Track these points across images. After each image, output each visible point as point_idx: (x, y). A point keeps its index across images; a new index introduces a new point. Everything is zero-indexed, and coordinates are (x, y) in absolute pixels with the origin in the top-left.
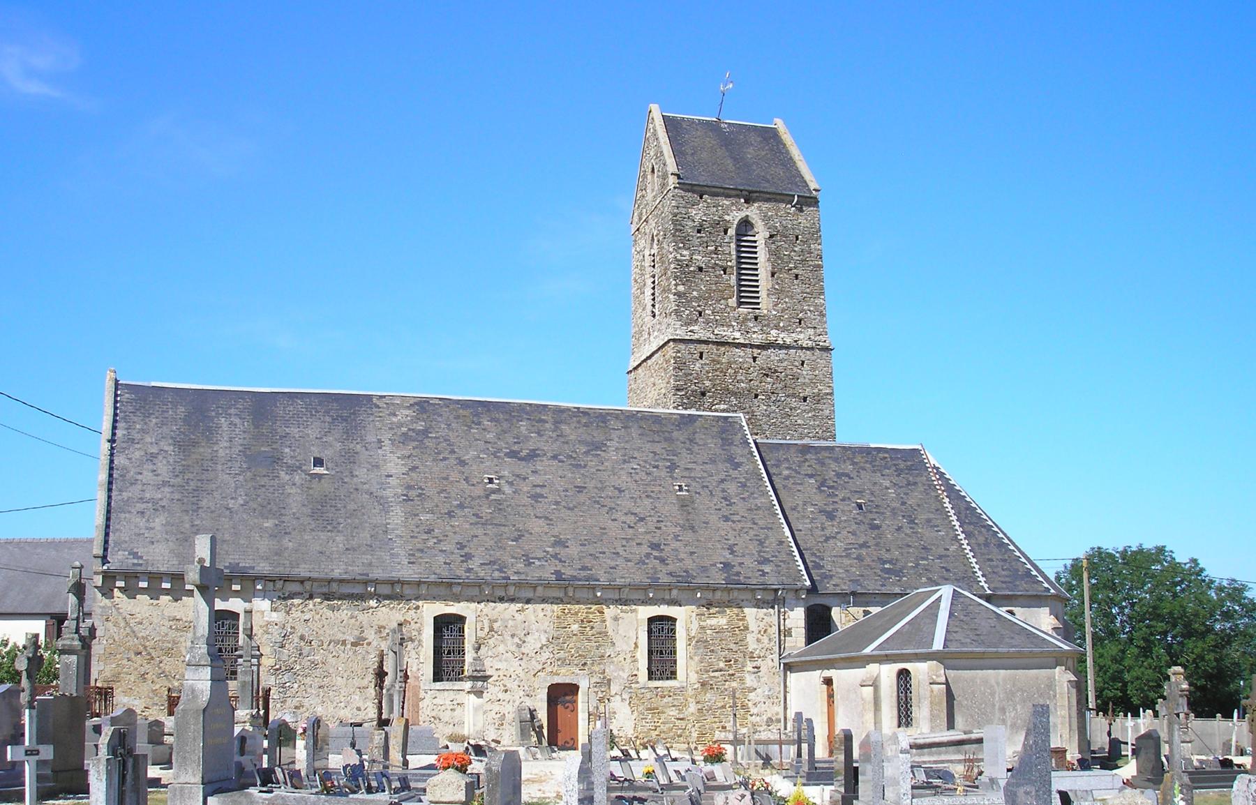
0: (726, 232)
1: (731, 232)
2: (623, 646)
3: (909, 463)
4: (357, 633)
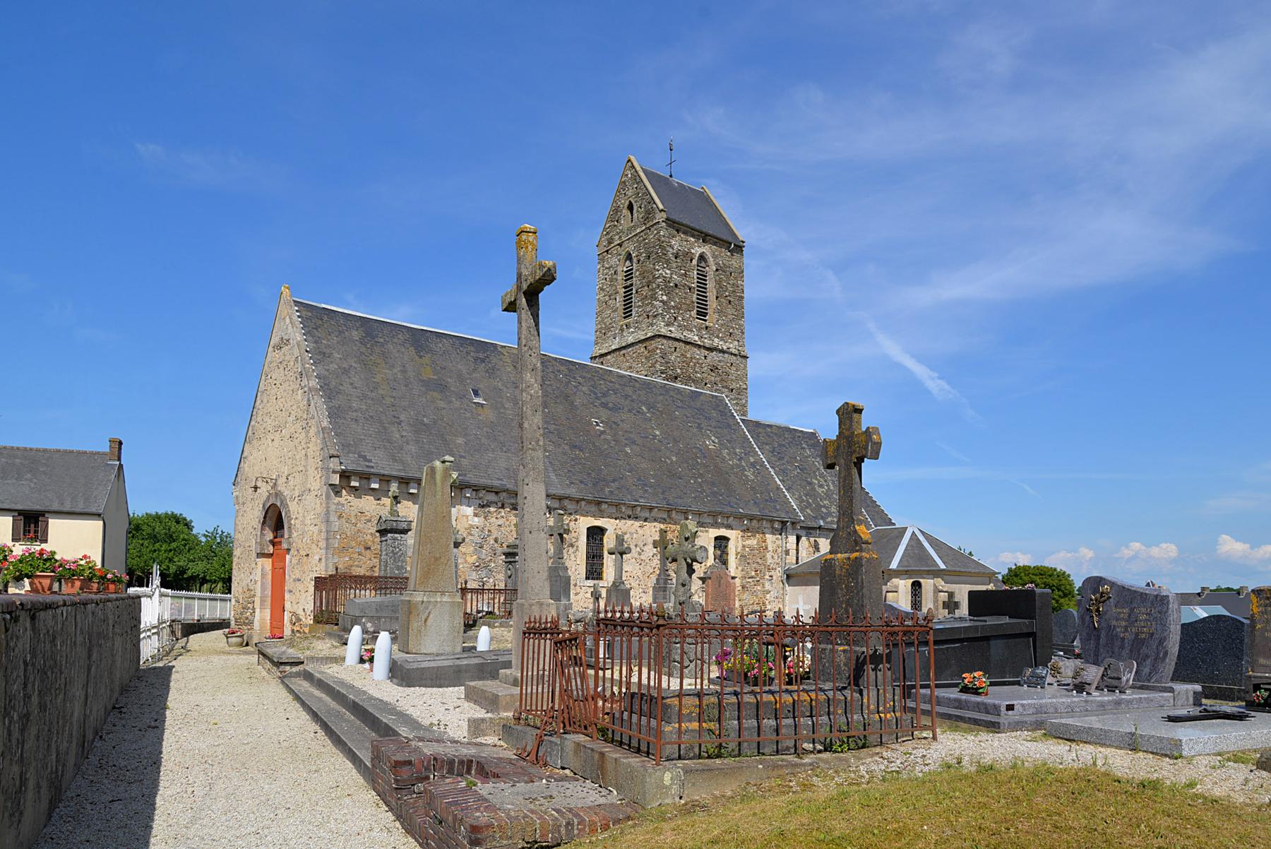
4: (543, 535)
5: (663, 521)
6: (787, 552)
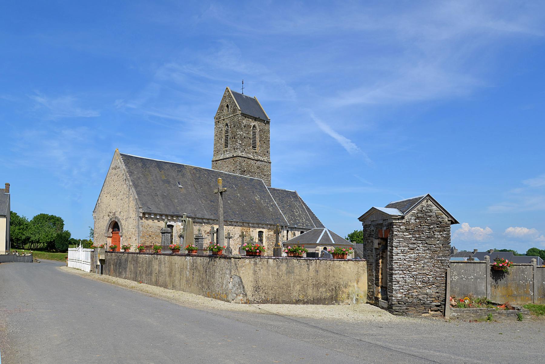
3: (294, 194)
5: (241, 226)
6: (283, 236)
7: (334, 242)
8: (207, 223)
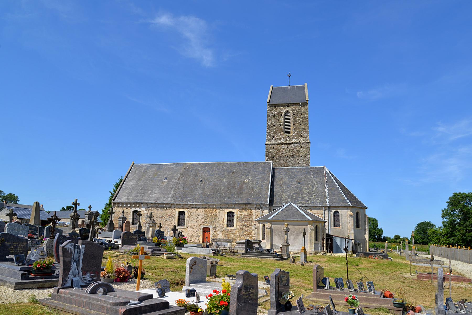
0: (281, 115)
1: (283, 115)
2: (221, 219)
5: (206, 208)
7: (310, 219)
8: (168, 207)
